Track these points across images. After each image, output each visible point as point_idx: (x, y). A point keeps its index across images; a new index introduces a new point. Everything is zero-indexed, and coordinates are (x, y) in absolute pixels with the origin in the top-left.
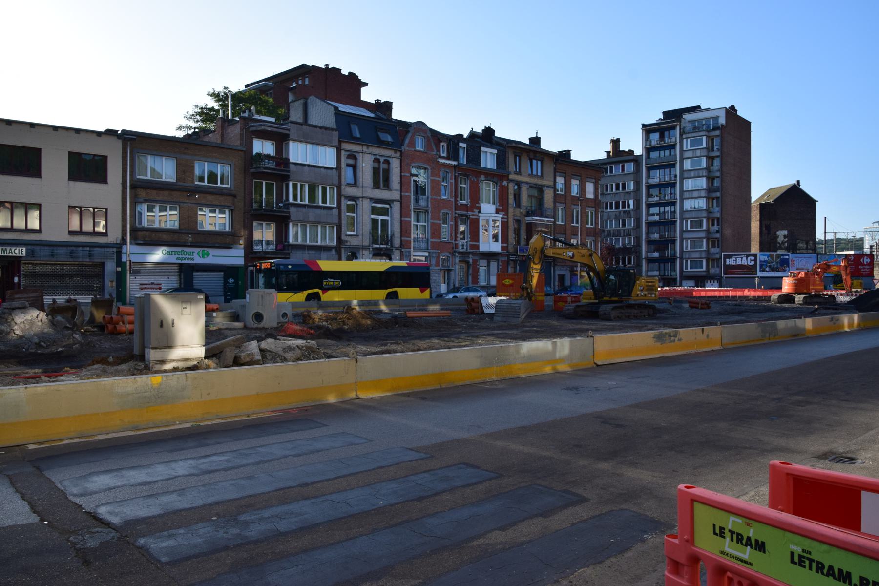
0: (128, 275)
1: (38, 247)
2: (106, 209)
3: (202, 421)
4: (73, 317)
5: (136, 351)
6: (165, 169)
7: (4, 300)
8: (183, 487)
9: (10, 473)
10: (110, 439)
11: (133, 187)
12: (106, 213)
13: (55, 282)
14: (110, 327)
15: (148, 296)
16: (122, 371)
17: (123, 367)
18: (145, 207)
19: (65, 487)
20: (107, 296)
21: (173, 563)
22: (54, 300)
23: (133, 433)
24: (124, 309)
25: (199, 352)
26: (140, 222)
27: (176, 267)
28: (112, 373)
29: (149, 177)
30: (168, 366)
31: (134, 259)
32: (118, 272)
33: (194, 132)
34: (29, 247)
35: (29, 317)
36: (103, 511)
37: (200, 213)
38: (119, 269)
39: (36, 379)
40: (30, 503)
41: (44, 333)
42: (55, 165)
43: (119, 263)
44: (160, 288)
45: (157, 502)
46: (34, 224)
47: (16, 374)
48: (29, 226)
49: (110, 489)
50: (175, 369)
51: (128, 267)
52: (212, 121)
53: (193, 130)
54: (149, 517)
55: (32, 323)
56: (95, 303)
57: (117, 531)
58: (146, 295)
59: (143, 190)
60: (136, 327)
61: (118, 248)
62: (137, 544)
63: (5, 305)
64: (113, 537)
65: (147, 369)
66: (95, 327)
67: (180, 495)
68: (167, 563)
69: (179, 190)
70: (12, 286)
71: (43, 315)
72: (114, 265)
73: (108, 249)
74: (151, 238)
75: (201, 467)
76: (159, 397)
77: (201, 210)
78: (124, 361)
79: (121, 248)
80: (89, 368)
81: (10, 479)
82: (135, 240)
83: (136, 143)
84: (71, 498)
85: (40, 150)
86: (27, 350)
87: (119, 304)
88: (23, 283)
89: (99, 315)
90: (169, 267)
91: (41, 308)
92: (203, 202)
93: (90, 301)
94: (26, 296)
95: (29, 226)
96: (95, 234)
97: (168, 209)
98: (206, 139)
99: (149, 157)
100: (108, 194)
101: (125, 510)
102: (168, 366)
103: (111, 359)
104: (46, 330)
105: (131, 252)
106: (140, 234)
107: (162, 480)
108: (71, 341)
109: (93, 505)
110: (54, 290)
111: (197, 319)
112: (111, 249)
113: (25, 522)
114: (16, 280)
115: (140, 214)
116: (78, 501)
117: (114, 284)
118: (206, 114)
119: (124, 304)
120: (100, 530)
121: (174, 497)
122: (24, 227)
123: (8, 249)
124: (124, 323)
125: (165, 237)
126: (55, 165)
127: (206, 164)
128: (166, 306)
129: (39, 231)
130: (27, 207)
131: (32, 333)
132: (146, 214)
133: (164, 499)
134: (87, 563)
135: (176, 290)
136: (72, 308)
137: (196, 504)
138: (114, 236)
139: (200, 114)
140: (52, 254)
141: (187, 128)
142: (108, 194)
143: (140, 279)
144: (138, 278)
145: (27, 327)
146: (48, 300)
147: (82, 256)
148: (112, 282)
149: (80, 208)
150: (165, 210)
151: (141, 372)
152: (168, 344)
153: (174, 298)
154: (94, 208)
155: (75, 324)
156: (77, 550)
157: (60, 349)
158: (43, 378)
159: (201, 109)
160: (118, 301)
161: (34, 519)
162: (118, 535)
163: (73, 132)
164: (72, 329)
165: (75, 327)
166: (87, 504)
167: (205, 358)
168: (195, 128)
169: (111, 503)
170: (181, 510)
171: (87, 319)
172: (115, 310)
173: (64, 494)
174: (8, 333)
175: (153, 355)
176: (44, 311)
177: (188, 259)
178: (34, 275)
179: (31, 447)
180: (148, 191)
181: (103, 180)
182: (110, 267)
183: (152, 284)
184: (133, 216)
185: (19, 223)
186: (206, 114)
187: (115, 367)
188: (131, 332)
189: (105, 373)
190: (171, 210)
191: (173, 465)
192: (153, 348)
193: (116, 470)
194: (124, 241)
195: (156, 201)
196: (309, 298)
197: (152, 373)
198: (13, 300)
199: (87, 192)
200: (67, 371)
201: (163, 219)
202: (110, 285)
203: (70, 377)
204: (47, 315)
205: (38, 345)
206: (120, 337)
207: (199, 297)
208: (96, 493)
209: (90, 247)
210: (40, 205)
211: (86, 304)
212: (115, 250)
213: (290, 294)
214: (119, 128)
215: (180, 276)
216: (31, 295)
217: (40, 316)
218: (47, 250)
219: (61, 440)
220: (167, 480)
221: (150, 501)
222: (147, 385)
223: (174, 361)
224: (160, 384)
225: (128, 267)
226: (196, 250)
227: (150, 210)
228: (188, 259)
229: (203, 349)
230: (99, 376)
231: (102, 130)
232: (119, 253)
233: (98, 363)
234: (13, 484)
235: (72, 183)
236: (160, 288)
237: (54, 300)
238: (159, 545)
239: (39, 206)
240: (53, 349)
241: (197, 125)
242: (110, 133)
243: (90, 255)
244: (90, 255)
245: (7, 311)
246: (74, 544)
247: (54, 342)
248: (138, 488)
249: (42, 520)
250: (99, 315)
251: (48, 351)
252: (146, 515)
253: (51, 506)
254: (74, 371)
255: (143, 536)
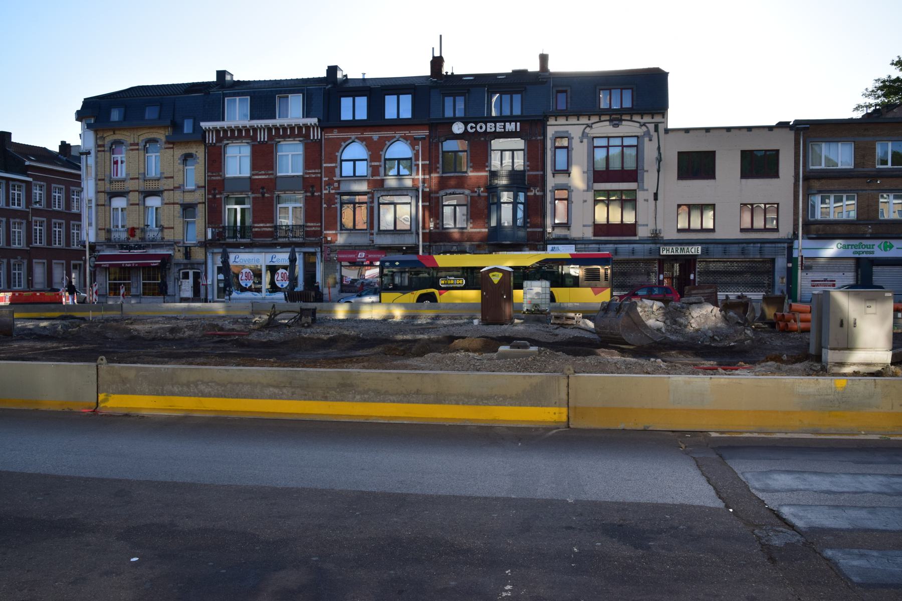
0: (800, 271)
1: (712, 246)
2: (778, 204)
3: (892, 435)
4: (745, 312)
5: (812, 350)
6: (841, 156)
7: (682, 296)
8: (874, 505)
9: (696, 456)
10: (789, 439)
11: (806, 179)
12: (778, 208)
13: (728, 279)
14: (782, 324)
15: (827, 293)
16: (797, 370)
17: (798, 366)
18: (818, 199)
19: (747, 479)
20: (777, 293)
21: (866, 586)
22: (727, 296)
23: (813, 436)
24: (795, 306)
25: (885, 357)
26: (813, 214)
27: (852, 262)
28: (786, 371)
29: (823, 166)
30: (847, 370)
31: (806, 254)
32: (788, 268)
33: (875, 110)
34: (704, 246)
35: (704, 312)
36: (786, 511)
37: (881, 200)
38: (790, 265)
39: (712, 370)
40: (715, 488)
41: (720, 328)
42: (728, 165)
43: (790, 259)
44: (834, 285)
45: (844, 514)
46: (709, 224)
47: (694, 365)
48: (692, 227)
49: (792, 491)
50: (856, 374)
51: (799, 263)
52: (896, 94)
53: (873, 108)
54: (837, 529)
55: (706, 317)
56: (767, 300)
57: (802, 536)
58: (825, 291)
59: (816, 181)
60: (813, 326)
61: (789, 243)
62: (825, 555)
63: (684, 300)
64: (798, 541)
65: (824, 371)
66: (766, 323)
67: (870, 513)
68: (859, 584)
69: (858, 177)
70: (688, 282)
71: (716, 310)
72: (785, 261)
73: (779, 245)
74: (825, 231)
75: (894, 486)
76: (843, 402)
77: (882, 196)
78: (798, 360)
79: (792, 243)
80: (763, 364)
81: (697, 462)
82: (808, 235)
83: (809, 132)
84: (753, 491)
85: (714, 153)
86: (702, 342)
87: (790, 301)
88: (697, 280)
89: (770, 312)
90: (845, 262)
91: (715, 303)
92: (886, 187)
93: (761, 297)
94: (701, 291)
95: (704, 226)
96: (703, 230)
97: (844, 199)
98: (890, 115)
99: (823, 145)
100: (780, 189)
101: (809, 516)
102: (847, 370)
103: (785, 357)
104: (719, 325)
105: (803, 247)
106: (813, 227)
107: (848, 493)
108: (743, 337)
109: (776, 503)
110: (726, 286)
111: (883, 319)
112: (782, 245)
113: (712, 505)
114: (692, 276)
115: (813, 207)
116: (760, 495)
117: (785, 280)
118: (890, 86)
119: (795, 301)
120: (784, 530)
121: (863, 514)
122: (762, 227)
123: (686, 248)
124: (795, 321)
125: (840, 229)
126: (728, 165)
127: (890, 144)
128: (848, 304)
129: (713, 230)
130: (702, 208)
131: (707, 327)
132: (819, 206)
133: (853, 513)
134: (772, 559)
135: (851, 287)
136: (743, 305)
137: (890, 527)
138: (785, 231)
139: (881, 88)
140: (725, 252)
141: (867, 107)
142: (780, 189)
143: (812, 276)
144: (810, 274)
145: (703, 321)
146: (721, 296)
147: (753, 253)
148: (782, 278)
149: (752, 205)
150: (841, 200)
151: (817, 373)
152: (849, 345)
153: (857, 295)
154: (765, 204)
155: (746, 320)
156: (763, 545)
157: (732, 344)
158: (720, 370)
159: (884, 82)
160: (789, 298)
161: (719, 504)
162: (803, 539)
163: (683, 133)
164: (743, 324)
165: (746, 323)
166: (771, 501)
167: (892, 364)
168: (876, 105)
169: (794, 505)
170: (873, 530)
171: (758, 315)
172: (786, 307)
173: (747, 487)
174: (686, 326)
175: (830, 356)
176: (717, 306)
177: (866, 252)
178: (706, 273)
179: (713, 435)
180: (823, 181)
181: (776, 175)
182: (781, 263)
183: (825, 280)
184: (806, 209)
185: (696, 224)
186: (890, 87)
187: (790, 366)
188: (806, 331)
189: (779, 371)
190: (848, 199)
191: (861, 478)
192: (831, 349)
193: (798, 472)
194: (795, 236)
195: (831, 191)
196: (421, 299)
197: (830, 375)
198: (690, 295)
199: (760, 189)
200: (741, 366)
201: (839, 210)
202: (780, 282)
203: (745, 372)
204: (721, 311)
205: (712, 339)
206: (791, 335)
207: (887, 295)
208: (778, 491)
209: (761, 243)
210: (714, 205)
211: (757, 301)
212: (786, 245)
213: (399, 294)
214: (791, 119)
215: (857, 271)
216: (706, 291)
217: (714, 311)
218: (720, 248)
219: (741, 433)
220: (856, 493)
221: (836, 512)
222: (831, 388)
223: (854, 364)
224: (845, 388)
225: (799, 263)
226: (877, 242)
227: (823, 202)
228: (866, 252)
229: (890, 354)
230: (773, 373)
231: (774, 124)
232: (790, 249)
233: (772, 360)
234: (699, 467)
235: (744, 181)
236: (834, 285)
237: (727, 296)
238: (850, 562)
239: (713, 206)
240: (726, 343)
241: (879, 101)
242: (782, 125)
243: (761, 251)
244: (761, 251)
245: (685, 305)
246: (759, 538)
247: (727, 336)
248: (822, 496)
249: (727, 507)
250: (770, 312)
251: (720, 345)
252: (833, 526)
253: (733, 493)
254: (747, 366)
255: (831, 548)
